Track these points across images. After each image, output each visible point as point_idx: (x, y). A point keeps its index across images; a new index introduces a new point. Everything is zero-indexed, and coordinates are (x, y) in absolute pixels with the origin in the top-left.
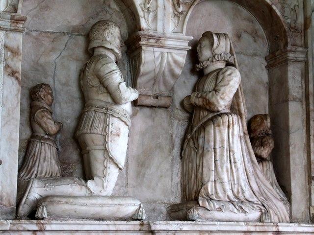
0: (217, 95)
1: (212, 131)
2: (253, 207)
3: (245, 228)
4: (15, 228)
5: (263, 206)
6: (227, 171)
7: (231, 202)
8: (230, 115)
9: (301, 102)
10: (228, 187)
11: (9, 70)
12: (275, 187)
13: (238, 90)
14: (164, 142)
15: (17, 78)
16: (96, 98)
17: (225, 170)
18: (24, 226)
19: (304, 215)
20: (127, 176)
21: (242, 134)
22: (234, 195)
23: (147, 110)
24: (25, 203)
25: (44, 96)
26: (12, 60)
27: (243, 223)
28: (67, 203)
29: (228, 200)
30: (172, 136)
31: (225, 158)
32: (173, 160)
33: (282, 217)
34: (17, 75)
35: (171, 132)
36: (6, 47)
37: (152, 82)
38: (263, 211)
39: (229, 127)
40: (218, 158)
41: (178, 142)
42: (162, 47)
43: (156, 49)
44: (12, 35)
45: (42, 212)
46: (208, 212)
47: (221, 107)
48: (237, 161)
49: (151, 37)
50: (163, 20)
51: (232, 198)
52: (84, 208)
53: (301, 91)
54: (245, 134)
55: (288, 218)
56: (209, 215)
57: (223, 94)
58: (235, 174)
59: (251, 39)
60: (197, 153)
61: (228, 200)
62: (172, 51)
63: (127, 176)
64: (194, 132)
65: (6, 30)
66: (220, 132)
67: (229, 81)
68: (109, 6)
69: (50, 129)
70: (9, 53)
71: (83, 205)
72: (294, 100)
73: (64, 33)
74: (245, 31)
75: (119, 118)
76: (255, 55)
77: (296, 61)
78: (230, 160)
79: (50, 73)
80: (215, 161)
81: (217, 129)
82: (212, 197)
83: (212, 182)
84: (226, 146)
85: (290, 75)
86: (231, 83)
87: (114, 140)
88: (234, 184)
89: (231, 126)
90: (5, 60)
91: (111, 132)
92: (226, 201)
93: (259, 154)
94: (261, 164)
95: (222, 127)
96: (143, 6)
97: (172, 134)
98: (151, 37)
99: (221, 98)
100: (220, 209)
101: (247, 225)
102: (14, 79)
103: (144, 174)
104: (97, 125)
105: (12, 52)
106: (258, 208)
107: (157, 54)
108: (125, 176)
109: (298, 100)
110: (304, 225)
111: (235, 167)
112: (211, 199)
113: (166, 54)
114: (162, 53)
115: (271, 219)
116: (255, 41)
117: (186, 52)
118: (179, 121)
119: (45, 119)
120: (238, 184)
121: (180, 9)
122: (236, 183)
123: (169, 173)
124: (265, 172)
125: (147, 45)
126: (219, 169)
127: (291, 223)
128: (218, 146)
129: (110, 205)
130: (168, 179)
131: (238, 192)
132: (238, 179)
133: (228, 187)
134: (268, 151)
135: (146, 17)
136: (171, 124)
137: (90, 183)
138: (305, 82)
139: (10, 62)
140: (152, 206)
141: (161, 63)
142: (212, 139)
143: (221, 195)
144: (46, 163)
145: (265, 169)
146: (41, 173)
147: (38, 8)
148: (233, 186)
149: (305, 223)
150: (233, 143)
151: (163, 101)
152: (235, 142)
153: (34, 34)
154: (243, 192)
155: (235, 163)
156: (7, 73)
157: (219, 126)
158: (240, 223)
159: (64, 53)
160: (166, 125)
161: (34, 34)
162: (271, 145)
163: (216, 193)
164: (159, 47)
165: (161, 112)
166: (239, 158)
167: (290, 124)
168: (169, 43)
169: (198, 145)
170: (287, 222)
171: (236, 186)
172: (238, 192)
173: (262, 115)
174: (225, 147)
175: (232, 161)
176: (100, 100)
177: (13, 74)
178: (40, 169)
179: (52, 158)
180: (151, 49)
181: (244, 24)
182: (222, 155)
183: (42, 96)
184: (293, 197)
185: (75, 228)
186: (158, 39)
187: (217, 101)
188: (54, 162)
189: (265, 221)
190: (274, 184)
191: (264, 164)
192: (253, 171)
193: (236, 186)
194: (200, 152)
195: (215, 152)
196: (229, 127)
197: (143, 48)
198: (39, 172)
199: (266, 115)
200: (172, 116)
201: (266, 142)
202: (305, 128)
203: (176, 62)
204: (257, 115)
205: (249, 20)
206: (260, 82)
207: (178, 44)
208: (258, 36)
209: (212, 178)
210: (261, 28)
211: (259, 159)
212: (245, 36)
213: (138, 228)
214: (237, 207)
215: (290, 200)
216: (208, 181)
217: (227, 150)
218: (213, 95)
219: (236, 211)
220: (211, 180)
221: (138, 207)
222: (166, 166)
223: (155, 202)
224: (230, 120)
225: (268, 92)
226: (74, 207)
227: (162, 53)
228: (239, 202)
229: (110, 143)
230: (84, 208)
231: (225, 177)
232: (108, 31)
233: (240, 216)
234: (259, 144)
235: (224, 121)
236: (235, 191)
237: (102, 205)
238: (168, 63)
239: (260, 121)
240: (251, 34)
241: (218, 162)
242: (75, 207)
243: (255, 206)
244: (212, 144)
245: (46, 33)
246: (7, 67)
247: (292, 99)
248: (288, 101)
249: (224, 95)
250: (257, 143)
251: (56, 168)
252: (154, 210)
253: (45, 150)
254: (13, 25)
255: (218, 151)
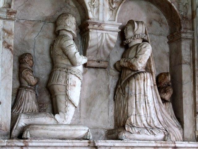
0: (137, 60)
1: (134, 83)
2: (160, 131)
3: (154, 145)
4: (9, 144)
5: (166, 130)
6: (143, 108)
7: (146, 128)
8: (145, 73)
9: (190, 64)
10: (144, 119)
11: (6, 44)
12: (173, 118)
13: (150, 57)
14: (103, 90)
15: (11, 50)
16: (61, 62)
17: (142, 108)
18: (15, 143)
19: (192, 136)
20: (80, 112)
21: (153, 85)
22: (148, 124)
23: (92, 70)
24: (16, 129)
25: (28, 61)
26: (8, 38)
27: (153, 142)
28: (42, 129)
29: (144, 127)
30: (108, 86)
31: (142, 100)
32: (109, 102)
33: (178, 138)
34: (11, 47)
35: (108, 84)
36: (4, 30)
37: (96, 52)
38: (166, 134)
39: (144, 80)
40: (137, 100)
41: (112, 90)
42: (102, 30)
43: (98, 31)
44: (7, 22)
45: (27, 134)
46: (131, 134)
47: (139, 68)
48: (149, 102)
49: (95, 23)
50: (103, 13)
51: (146, 125)
52: (53, 132)
53: (190, 58)
54: (154, 85)
55: (181, 138)
56: (132, 136)
57: (141, 59)
58: (148, 110)
59: (158, 25)
60: (124, 97)
61: (144, 127)
62: (108, 32)
63: (80, 112)
64: (122, 84)
65: (4, 19)
66: (139, 83)
67: (144, 51)
68: (69, 4)
69: (32, 82)
70: (6, 34)
71: (52, 130)
72: (186, 63)
73: (40, 21)
74: (155, 20)
75: (75, 75)
76: (161, 35)
77: (187, 39)
78: (145, 102)
79: (32, 46)
80: (136, 102)
81: (137, 82)
82: (133, 125)
83: (134, 115)
84: (142, 93)
85: (183, 47)
86: (146, 53)
87: (72, 89)
88: (148, 117)
89: (146, 80)
90: (3, 38)
91: (70, 84)
92: (143, 128)
93: (163, 98)
94: (164, 104)
95: (140, 81)
96: (90, 4)
97: (109, 85)
98: (95, 23)
99: (139, 62)
100: (139, 133)
101: (156, 142)
102: (9, 50)
103: (91, 110)
104: (61, 79)
105: (8, 33)
106: (163, 132)
107: (99, 34)
108: (79, 111)
109: (188, 63)
110: (192, 143)
111: (148, 106)
112: (133, 126)
113: (105, 34)
114: (102, 34)
115: (171, 139)
116: (161, 26)
117: (117, 33)
118: (113, 77)
119: (28, 75)
120: (150, 117)
121: (114, 6)
122: (149, 116)
123: (107, 109)
124: (167, 109)
125: (93, 29)
126: (138, 107)
127: (183, 141)
128: (137, 93)
129: (69, 130)
130: (106, 114)
131: (150, 122)
132: (150, 114)
133: (144, 119)
134: (169, 95)
135: (92, 11)
136: (108, 79)
137: (57, 116)
138: (193, 52)
139: (6, 39)
140: (96, 131)
141: (102, 40)
142: (134, 88)
143: (139, 123)
144: (29, 103)
145: (167, 107)
146: (26, 110)
147: (24, 5)
148: (147, 118)
149: (192, 142)
150: (147, 90)
151: (103, 64)
152: (148, 90)
153: (22, 21)
154: (153, 122)
155: (148, 103)
156: (4, 47)
157: (138, 80)
158: (151, 141)
159: (40, 34)
160: (104, 79)
161: (22, 21)
162: (171, 92)
163: (137, 122)
164: (100, 30)
165: (101, 71)
166: (151, 100)
167: (183, 79)
168: (106, 27)
169: (125, 92)
170: (181, 141)
171: (149, 118)
172: (150, 122)
173: (165, 73)
174: (142, 93)
175: (146, 102)
176: (63, 64)
177: (8, 47)
178: (25, 107)
179: (33, 100)
180: (95, 31)
181: (154, 15)
182: (140, 98)
183: (27, 61)
184: (185, 125)
185: (47, 144)
186: (100, 25)
187: (137, 64)
188: (34, 103)
189: (167, 140)
190: (173, 117)
191: (167, 104)
192: (160, 108)
193: (149, 118)
194: (126, 96)
195: (136, 96)
196: (144, 80)
197: (90, 30)
198: (25, 109)
199: (167, 73)
200: (108, 74)
201: (168, 90)
202: (192, 81)
203: (111, 39)
204: (162, 73)
205: (157, 13)
206: (164, 52)
207: (112, 28)
208: (163, 23)
209: (134, 113)
210: (165, 18)
211: (163, 101)
212: (155, 23)
213: (87, 144)
214: (150, 132)
215: (183, 127)
216: (131, 115)
217: (143, 95)
218: (134, 60)
219: (149, 134)
220: (133, 114)
221: (87, 131)
222: (105, 105)
223: (98, 128)
224: (145, 76)
225: (169, 58)
226: (46, 131)
227: (102, 34)
228: (151, 128)
229: (69, 91)
230: (53, 132)
231: (142, 112)
232: (68, 20)
233: (152, 137)
234: (163, 91)
235: (141, 77)
236: (148, 121)
237: (64, 130)
238: (106, 40)
239: (164, 77)
240: (158, 22)
241: (138, 103)
242: (48, 131)
243: (161, 130)
244: (134, 91)
245: (29, 21)
246: (4, 42)
247: (184, 63)
248: (182, 64)
249: (142, 60)
250: (162, 91)
251: (35, 107)
252: (97, 133)
253: (28, 95)
254: (8, 16)
255: (137, 96)
